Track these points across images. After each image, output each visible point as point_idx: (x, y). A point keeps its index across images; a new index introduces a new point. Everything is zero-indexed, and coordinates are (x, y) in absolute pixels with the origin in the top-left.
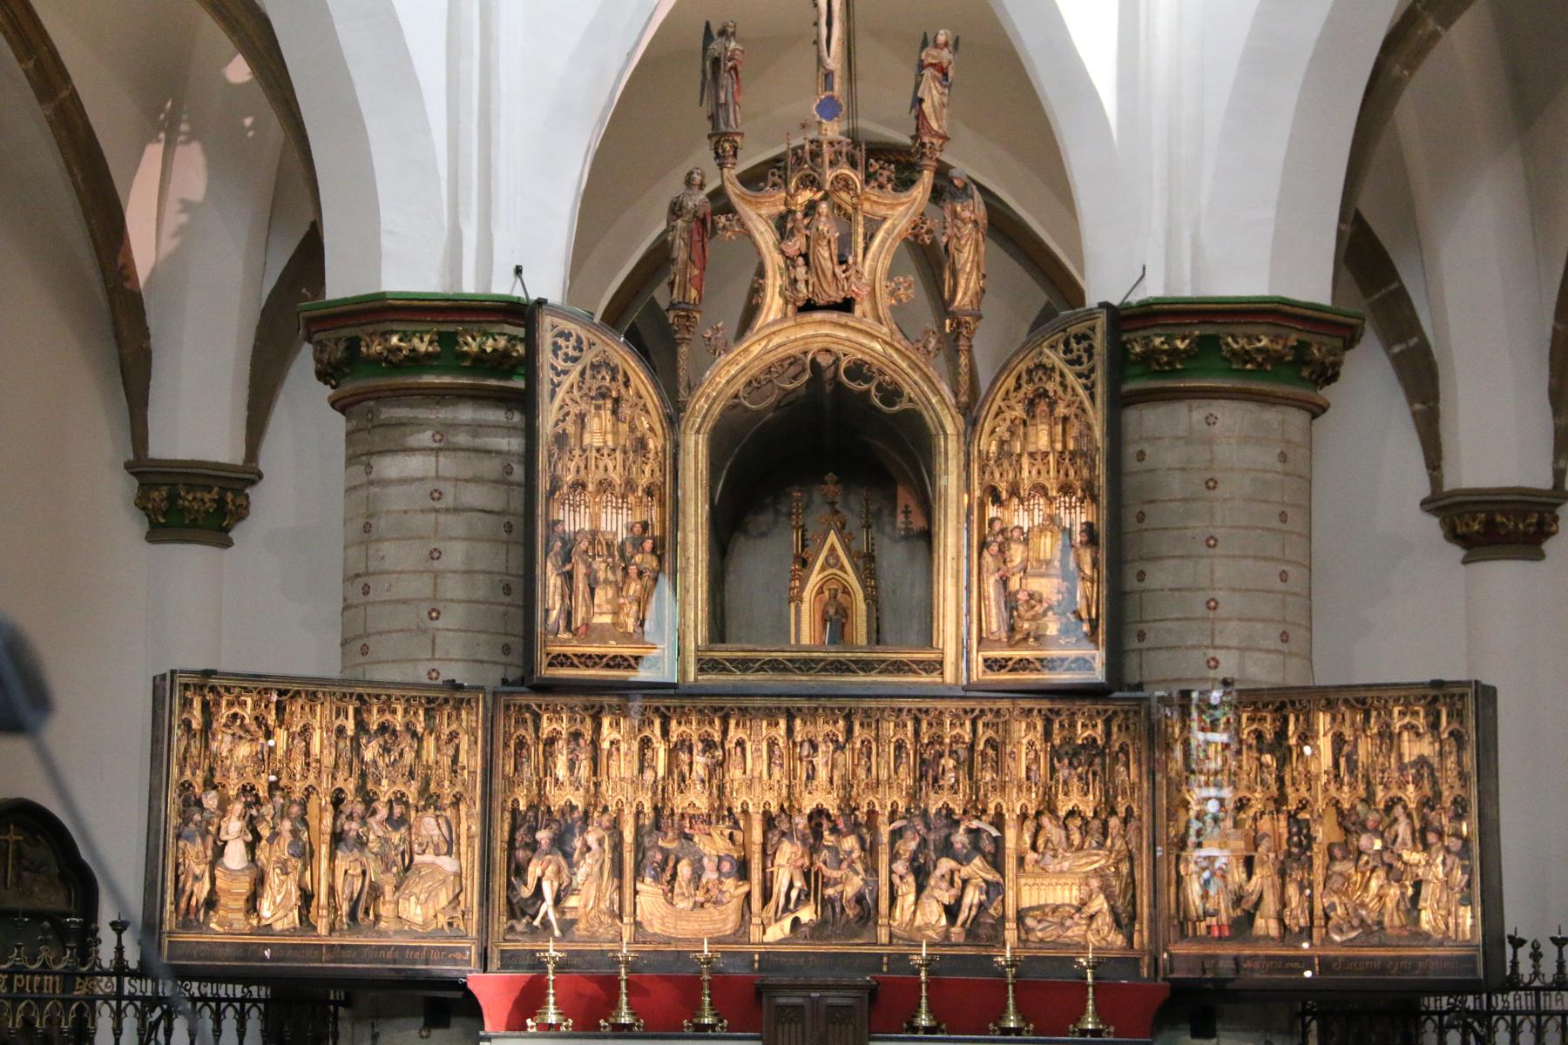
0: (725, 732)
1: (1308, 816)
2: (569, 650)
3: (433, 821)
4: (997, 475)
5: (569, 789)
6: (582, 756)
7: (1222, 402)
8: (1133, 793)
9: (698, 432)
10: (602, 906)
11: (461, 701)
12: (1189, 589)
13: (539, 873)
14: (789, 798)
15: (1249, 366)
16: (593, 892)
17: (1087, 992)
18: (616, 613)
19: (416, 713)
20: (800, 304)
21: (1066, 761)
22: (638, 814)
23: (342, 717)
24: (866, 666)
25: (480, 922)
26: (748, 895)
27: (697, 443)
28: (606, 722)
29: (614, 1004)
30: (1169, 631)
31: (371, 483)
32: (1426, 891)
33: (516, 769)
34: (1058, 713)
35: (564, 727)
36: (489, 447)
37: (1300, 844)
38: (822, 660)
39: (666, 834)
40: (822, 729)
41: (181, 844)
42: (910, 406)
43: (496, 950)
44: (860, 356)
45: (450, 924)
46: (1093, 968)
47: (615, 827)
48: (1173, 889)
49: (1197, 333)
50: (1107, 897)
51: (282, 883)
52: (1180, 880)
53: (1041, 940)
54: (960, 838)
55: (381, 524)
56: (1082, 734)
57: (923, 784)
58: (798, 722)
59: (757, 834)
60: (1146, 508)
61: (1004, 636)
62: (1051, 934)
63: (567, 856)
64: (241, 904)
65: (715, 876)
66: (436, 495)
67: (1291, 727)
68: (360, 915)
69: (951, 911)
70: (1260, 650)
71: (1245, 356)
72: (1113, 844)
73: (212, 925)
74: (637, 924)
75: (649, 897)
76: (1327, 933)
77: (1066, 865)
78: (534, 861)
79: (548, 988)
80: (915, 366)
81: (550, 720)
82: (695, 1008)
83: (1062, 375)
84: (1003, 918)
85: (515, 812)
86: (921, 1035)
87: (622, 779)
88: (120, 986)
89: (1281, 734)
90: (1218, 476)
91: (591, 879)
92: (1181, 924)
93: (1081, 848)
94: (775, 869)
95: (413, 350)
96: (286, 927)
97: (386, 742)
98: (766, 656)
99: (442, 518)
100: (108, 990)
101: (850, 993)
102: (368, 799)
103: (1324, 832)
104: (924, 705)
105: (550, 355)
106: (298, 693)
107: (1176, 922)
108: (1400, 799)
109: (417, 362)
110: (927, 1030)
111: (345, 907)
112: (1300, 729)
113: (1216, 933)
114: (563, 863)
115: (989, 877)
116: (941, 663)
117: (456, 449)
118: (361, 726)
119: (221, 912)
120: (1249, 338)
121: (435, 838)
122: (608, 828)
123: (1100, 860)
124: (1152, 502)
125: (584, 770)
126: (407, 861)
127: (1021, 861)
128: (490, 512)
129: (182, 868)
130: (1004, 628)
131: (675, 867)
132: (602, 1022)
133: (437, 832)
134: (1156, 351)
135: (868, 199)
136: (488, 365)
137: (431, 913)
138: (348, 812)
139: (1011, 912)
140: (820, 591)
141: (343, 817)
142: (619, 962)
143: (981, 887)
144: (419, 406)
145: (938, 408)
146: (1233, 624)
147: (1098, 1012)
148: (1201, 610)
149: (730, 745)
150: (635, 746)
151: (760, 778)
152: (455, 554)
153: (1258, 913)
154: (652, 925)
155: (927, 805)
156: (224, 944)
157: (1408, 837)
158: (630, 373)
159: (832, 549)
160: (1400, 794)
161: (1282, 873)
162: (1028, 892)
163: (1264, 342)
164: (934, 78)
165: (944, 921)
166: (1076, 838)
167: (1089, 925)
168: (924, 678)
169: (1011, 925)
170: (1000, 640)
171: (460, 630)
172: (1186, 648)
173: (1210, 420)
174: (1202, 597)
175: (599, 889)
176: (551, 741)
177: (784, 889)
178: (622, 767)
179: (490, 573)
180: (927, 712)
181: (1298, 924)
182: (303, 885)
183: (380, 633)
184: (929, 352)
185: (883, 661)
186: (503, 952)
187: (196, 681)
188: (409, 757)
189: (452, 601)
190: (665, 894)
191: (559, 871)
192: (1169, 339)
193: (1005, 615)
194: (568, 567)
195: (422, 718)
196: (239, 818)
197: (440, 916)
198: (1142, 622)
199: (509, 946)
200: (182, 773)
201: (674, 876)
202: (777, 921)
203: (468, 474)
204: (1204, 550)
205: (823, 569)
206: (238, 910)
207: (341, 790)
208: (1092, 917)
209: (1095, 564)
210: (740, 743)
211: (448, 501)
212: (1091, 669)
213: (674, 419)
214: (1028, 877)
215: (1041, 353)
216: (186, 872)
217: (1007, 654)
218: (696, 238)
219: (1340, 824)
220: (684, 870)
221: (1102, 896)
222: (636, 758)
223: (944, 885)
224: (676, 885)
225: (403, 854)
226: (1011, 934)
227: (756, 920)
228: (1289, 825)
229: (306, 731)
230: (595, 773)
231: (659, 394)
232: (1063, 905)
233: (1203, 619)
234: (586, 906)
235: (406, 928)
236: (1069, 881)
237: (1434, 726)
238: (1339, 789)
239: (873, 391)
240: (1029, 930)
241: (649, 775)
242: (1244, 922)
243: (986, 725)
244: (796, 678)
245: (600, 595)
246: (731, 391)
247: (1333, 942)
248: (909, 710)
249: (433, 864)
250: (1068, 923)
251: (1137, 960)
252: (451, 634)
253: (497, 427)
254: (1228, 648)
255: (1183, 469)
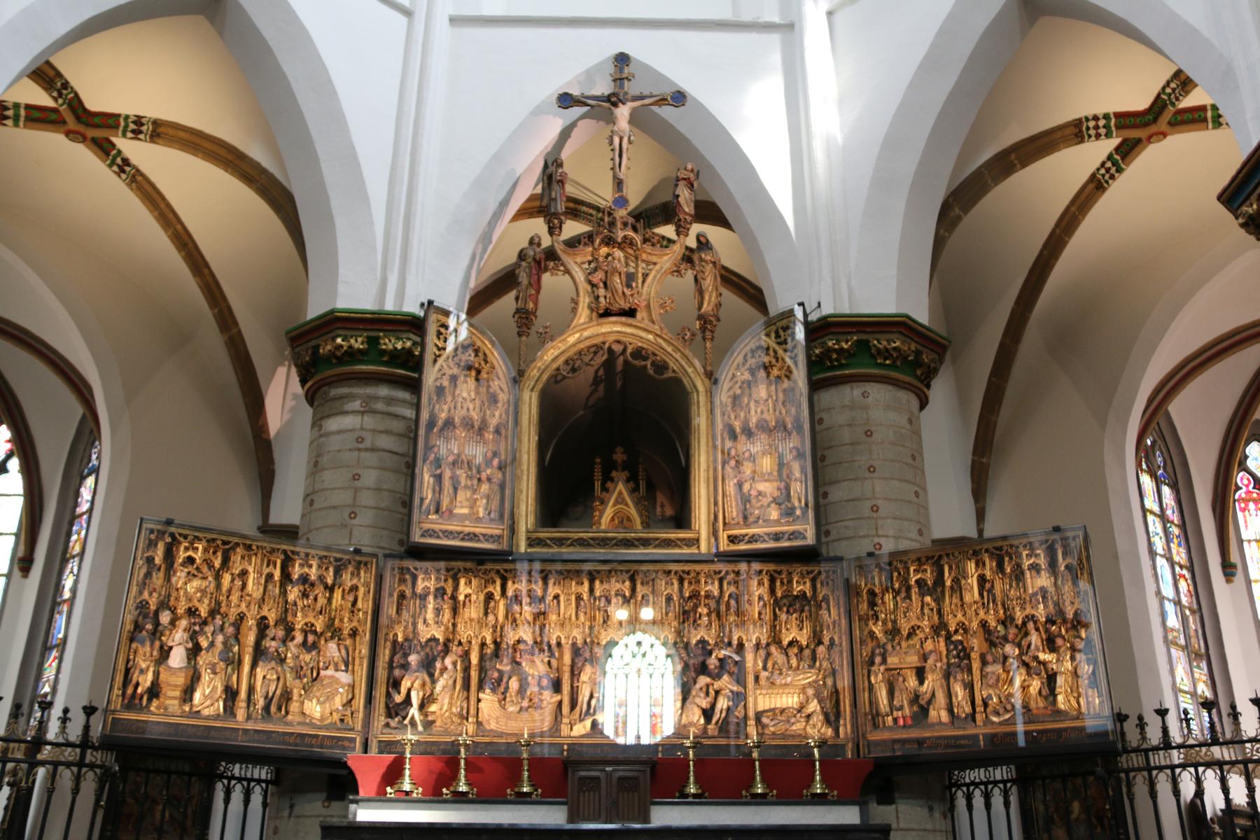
0: (545, 590)
1: (960, 638)
2: (436, 527)
3: (335, 646)
4: (733, 416)
5: (434, 626)
6: (445, 606)
7: (872, 384)
8: (834, 627)
9: (532, 390)
10: (454, 710)
11: (360, 563)
12: (859, 499)
13: (409, 684)
14: (590, 635)
15: (888, 362)
16: (446, 701)
17: (814, 766)
18: (471, 507)
19: (327, 569)
20: (601, 312)
21: (785, 609)
22: (483, 645)
23: (271, 567)
24: (646, 543)
25: (364, 720)
26: (560, 703)
27: (531, 398)
28: (462, 581)
29: (454, 777)
30: (847, 527)
31: (321, 436)
32: (1060, 680)
33: (397, 612)
34: (780, 573)
35: (432, 584)
36: (398, 413)
37: (958, 656)
38: (614, 538)
39: (502, 661)
40: (615, 585)
41: (134, 645)
42: (673, 375)
43: (375, 740)
44: (640, 344)
45: (342, 720)
46: (819, 747)
47: (466, 655)
48: (866, 694)
49: (855, 338)
50: (819, 702)
51: (212, 680)
52: (871, 687)
53: (774, 733)
54: (712, 662)
55: (325, 460)
56: (797, 588)
57: (686, 625)
58: (597, 583)
59: (567, 659)
60: (826, 453)
61: (741, 520)
62: (781, 728)
63: (431, 675)
64: (177, 693)
65: (536, 689)
66: (360, 440)
67: (947, 574)
68: (273, 709)
69: (708, 714)
70: (907, 538)
71: (886, 353)
72: (821, 665)
73: (152, 709)
74: (479, 724)
75: (488, 701)
76: (987, 716)
77: (789, 679)
78: (406, 677)
79: (405, 764)
80: (677, 349)
81: (423, 579)
82: (516, 780)
83: (775, 352)
84: (746, 717)
85: (395, 642)
86: (690, 800)
87: (471, 620)
88: (83, 755)
89: (939, 580)
90: (873, 429)
91: (446, 689)
92: (873, 718)
93: (798, 668)
94: (580, 684)
95: (350, 347)
96: (212, 713)
97: (305, 590)
98: (576, 536)
99: (363, 454)
100: (71, 759)
101: (636, 767)
102: (289, 630)
103: (976, 644)
104: (686, 568)
105: (435, 337)
106: (237, 545)
107: (870, 717)
108: (1033, 616)
109: (352, 356)
110: (695, 796)
111: (261, 703)
112: (953, 574)
113: (901, 722)
114: (427, 679)
115: (735, 689)
116: (698, 540)
117: (374, 412)
118: (286, 577)
119: (161, 700)
120: (889, 341)
121: (336, 659)
122: (461, 656)
123: (809, 677)
124: (830, 447)
125: (447, 615)
126: (315, 675)
127: (757, 678)
128: (396, 453)
129: (131, 663)
130: (741, 516)
131: (507, 683)
132: (444, 790)
133: (337, 654)
134: (830, 350)
135: (645, 252)
136: (399, 361)
137: (328, 711)
138: (272, 636)
139: (751, 714)
140: (613, 519)
141: (268, 638)
142: (460, 745)
143: (728, 697)
144: (353, 386)
145: (692, 375)
146: (889, 521)
147: (823, 781)
148: (867, 513)
149: (549, 598)
150: (482, 597)
151: (570, 619)
152: (370, 478)
153: (931, 707)
154: (489, 724)
155: (689, 638)
156: (159, 723)
157: (1039, 643)
158: (487, 352)
159: (620, 493)
160: (1033, 612)
161: (947, 675)
162: (762, 700)
163: (898, 344)
164: (686, 186)
165: (702, 721)
166: (794, 662)
167: (807, 722)
168: (686, 551)
169: (752, 722)
170: (738, 523)
171: (368, 526)
172: (860, 537)
173: (865, 394)
174: (869, 504)
175: (451, 698)
176: (423, 597)
177: (586, 699)
178: (473, 612)
179: (395, 492)
180: (688, 573)
181: (964, 711)
182: (230, 684)
183: (317, 529)
184: (685, 341)
185: (657, 539)
186: (380, 741)
187: (159, 527)
188: (322, 601)
189: (365, 507)
190: (500, 702)
191: (424, 685)
192: (838, 342)
193: (741, 507)
194: (438, 471)
195: (331, 573)
196: (185, 630)
197: (334, 714)
198: (827, 524)
199: (385, 738)
200: (141, 593)
201: (507, 688)
202: (581, 721)
203: (381, 428)
204: (867, 475)
205: (614, 505)
206: (174, 698)
207: (264, 618)
208: (809, 716)
209: (803, 470)
210: (557, 597)
211: (368, 444)
212: (805, 538)
213: (518, 378)
214: (761, 689)
215: (760, 339)
216: (135, 666)
217: (744, 531)
218: (534, 271)
219: (986, 640)
220: (514, 684)
221: (816, 701)
222: (482, 605)
223: (702, 695)
224: (508, 695)
225: (312, 669)
226: (752, 730)
227: (565, 720)
228: (946, 645)
229: (244, 573)
230: (454, 618)
231: (506, 365)
232: (788, 708)
233: (869, 518)
234: (441, 709)
235: (308, 721)
236: (792, 691)
237: (1053, 565)
238: (987, 612)
239: (649, 366)
240: (764, 726)
241: (491, 618)
242: (922, 709)
243: (729, 583)
244: (597, 551)
245: (461, 495)
246: (555, 366)
247: (993, 723)
248: (676, 573)
249: (333, 677)
250: (793, 720)
251: (844, 746)
252: (362, 528)
253: (404, 401)
254: (887, 536)
255: (850, 425)
